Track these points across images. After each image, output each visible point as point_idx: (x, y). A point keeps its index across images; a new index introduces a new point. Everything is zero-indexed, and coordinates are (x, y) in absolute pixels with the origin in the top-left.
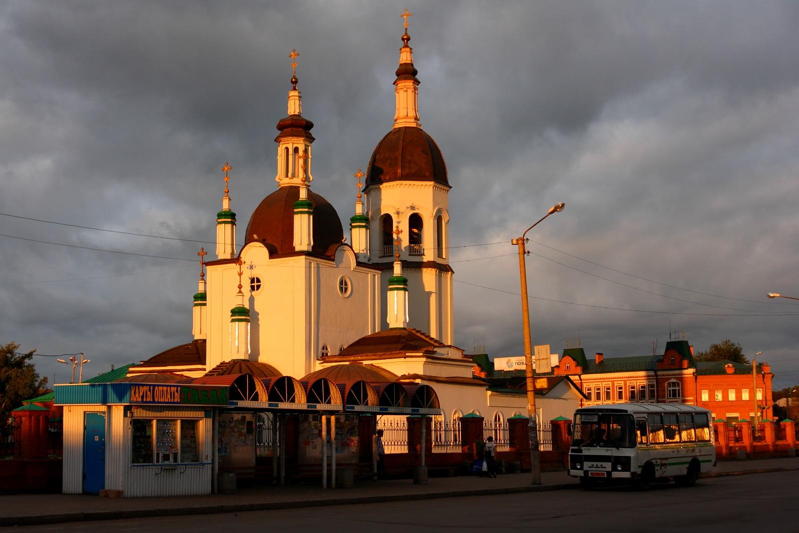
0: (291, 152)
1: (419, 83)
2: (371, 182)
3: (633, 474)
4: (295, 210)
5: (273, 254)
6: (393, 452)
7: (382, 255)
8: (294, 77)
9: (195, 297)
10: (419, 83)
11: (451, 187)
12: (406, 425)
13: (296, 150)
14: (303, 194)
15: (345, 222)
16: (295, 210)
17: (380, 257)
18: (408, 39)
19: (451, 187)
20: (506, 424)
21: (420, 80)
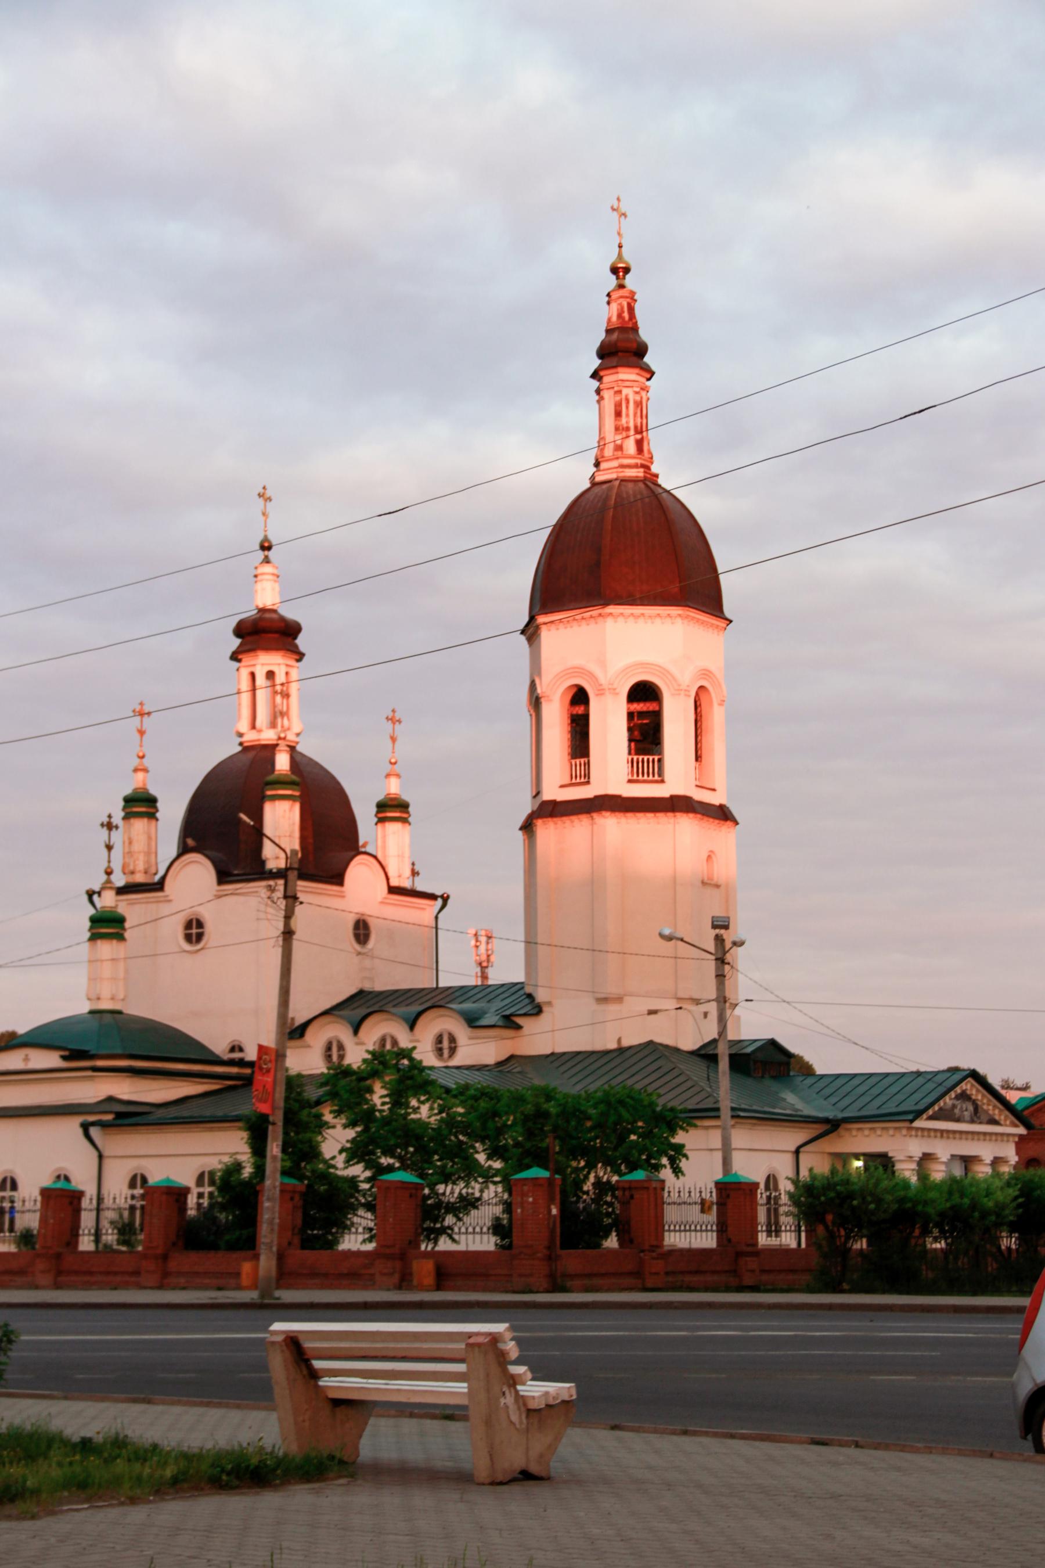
0: (261, 680)
1: (652, 373)
2: (539, 610)
3: (376, 1229)
4: (269, 793)
5: (224, 876)
6: (472, 1248)
7: (567, 781)
8: (266, 539)
9: (243, 630)
10: (652, 373)
11: (731, 621)
12: (714, 1194)
13: (270, 675)
14: (282, 762)
15: (364, 813)
16: (269, 793)
17: (562, 786)
18: (627, 270)
19: (731, 621)
20: (711, 1192)
21: (654, 368)
